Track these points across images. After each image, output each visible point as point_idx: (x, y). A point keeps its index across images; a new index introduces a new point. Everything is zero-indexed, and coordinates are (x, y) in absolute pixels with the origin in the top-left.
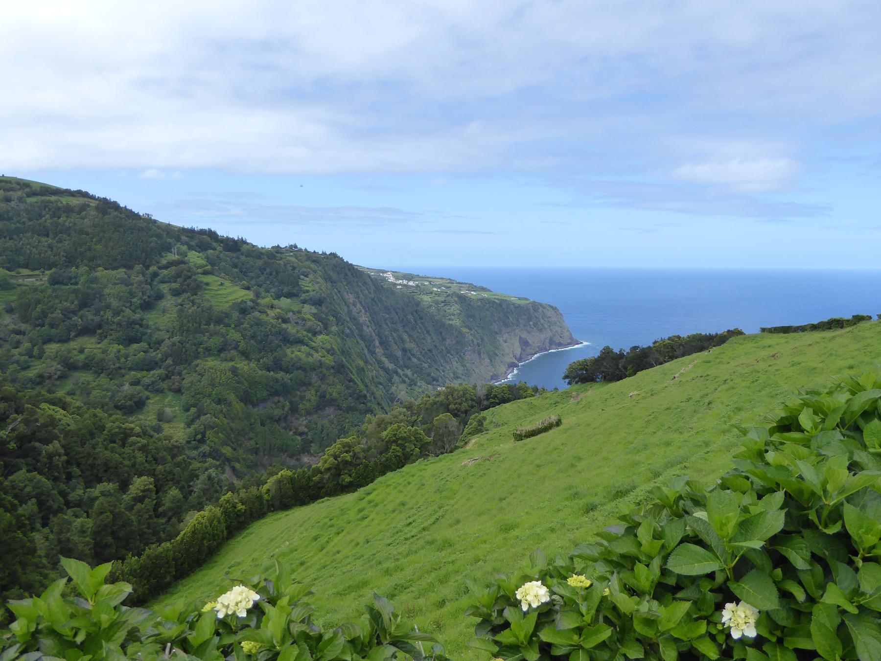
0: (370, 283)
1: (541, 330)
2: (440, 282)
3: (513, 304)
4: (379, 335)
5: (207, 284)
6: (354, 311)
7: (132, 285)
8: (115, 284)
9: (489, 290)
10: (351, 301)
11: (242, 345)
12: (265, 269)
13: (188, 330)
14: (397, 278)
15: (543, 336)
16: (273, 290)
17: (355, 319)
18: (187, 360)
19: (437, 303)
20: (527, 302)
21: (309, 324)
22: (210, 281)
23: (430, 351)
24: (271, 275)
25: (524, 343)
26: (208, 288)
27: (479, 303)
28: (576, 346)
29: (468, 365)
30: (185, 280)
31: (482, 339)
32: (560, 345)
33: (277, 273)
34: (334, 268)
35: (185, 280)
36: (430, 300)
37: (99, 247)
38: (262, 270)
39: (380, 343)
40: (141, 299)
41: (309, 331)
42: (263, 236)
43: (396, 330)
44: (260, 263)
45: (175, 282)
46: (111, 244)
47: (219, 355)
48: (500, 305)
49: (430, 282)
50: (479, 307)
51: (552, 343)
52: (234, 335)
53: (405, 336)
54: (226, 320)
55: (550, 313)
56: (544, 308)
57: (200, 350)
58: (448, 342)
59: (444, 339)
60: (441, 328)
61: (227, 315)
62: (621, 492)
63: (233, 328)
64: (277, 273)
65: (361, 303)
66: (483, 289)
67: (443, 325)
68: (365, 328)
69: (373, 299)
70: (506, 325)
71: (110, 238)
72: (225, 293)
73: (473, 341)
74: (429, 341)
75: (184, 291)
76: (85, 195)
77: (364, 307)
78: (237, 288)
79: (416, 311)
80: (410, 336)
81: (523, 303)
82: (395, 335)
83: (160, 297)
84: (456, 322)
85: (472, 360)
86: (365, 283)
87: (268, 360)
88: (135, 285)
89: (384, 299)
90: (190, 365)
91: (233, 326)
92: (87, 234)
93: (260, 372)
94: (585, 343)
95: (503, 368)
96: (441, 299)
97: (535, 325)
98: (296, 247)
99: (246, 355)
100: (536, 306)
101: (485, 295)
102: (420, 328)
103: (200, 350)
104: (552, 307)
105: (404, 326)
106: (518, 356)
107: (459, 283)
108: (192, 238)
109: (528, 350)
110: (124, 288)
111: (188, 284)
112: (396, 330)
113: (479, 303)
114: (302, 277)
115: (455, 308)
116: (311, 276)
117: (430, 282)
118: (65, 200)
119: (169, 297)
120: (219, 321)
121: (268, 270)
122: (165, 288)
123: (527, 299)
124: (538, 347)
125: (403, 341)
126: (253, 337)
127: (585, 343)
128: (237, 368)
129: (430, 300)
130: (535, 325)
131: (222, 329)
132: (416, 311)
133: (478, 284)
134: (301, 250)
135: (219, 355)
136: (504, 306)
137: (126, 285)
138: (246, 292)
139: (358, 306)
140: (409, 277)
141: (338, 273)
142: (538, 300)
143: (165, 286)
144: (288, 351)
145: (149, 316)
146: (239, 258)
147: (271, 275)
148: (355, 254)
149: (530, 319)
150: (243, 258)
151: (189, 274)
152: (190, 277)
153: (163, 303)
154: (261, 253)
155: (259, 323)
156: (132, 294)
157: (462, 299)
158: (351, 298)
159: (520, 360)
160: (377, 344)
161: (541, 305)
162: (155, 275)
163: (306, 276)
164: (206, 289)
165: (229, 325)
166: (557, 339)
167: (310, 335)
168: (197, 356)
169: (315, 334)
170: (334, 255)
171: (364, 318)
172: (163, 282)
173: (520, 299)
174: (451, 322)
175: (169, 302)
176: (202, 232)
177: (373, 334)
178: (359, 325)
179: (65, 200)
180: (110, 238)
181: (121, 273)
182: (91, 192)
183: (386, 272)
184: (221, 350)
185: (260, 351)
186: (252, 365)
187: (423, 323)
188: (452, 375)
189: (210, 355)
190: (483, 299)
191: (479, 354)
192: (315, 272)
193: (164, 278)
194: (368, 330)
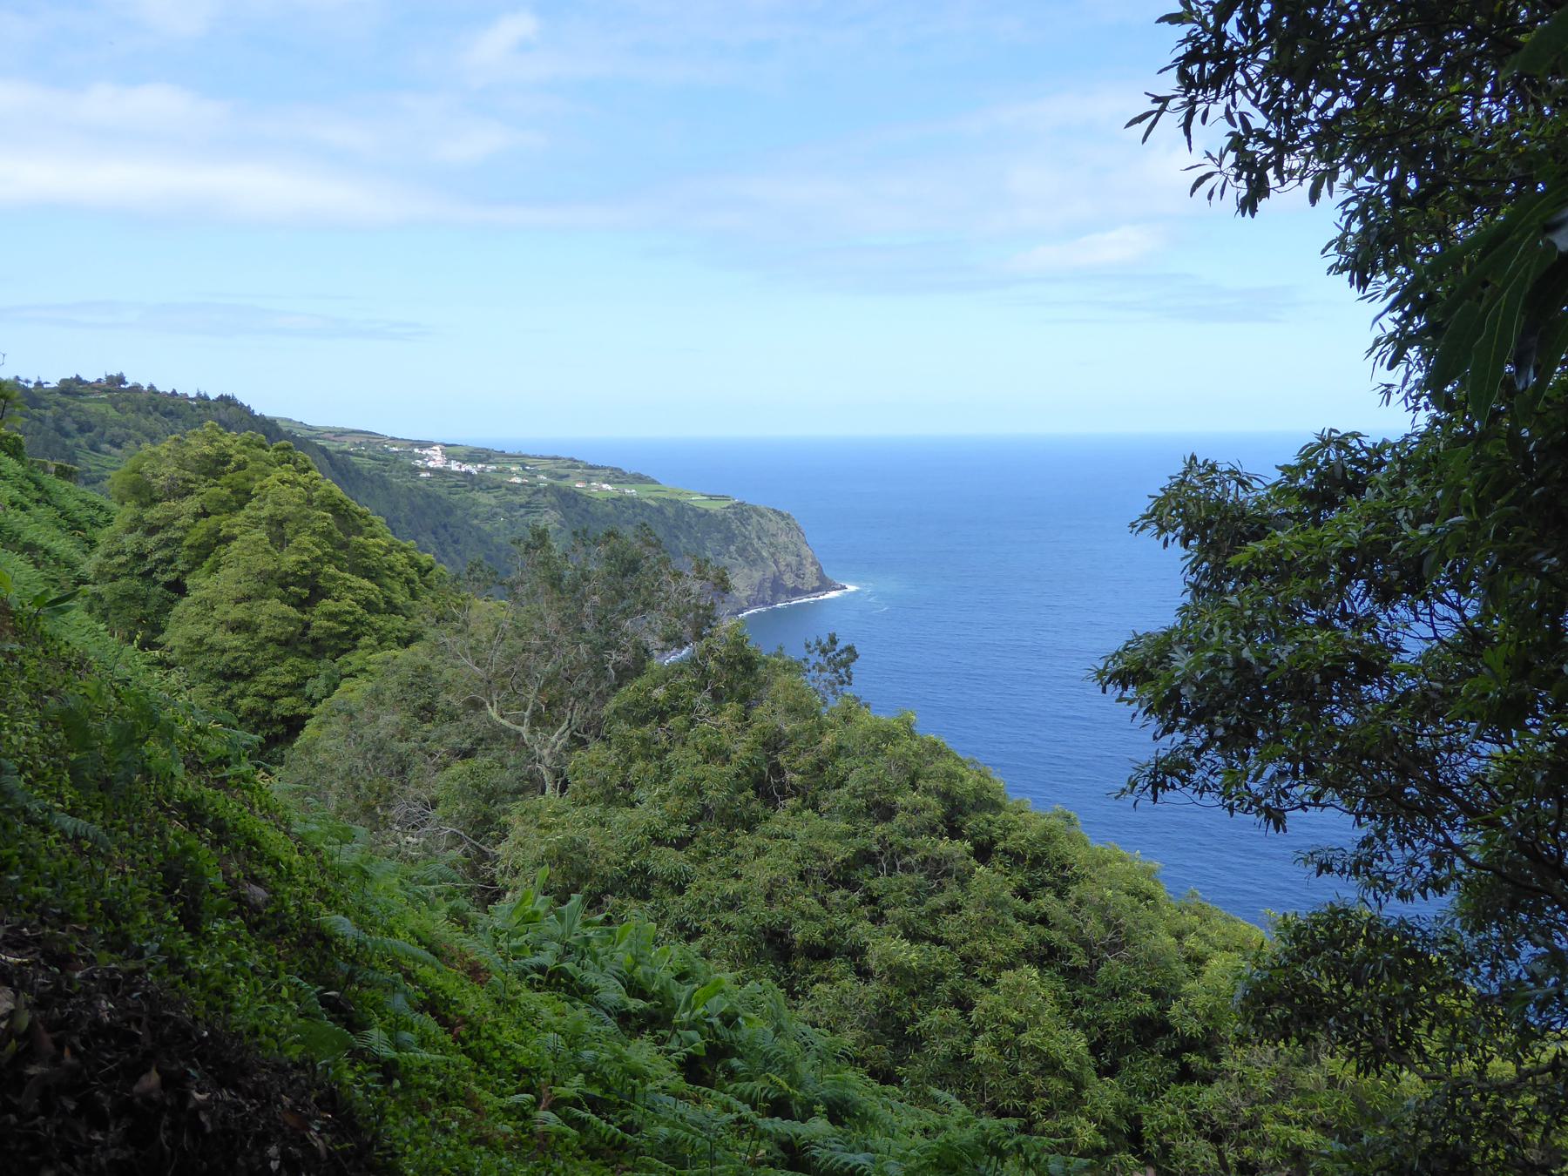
1: (752, 564)
2: (550, 465)
3: (693, 509)
9: (654, 482)
15: (757, 575)
19: (510, 508)
20: (726, 504)
27: (610, 508)
28: (832, 594)
32: (796, 592)
36: (494, 502)
48: (660, 510)
50: (608, 515)
51: (777, 588)
62: (569, 990)
66: (639, 479)
79: (445, 526)
81: (715, 507)
94: (851, 588)
96: (518, 499)
98: (121, 379)
100: (743, 512)
104: (779, 513)
107: (592, 468)
113: (610, 508)
123: (725, 498)
124: (747, 599)
127: (851, 588)
129: (494, 502)
130: (742, 552)
132: (445, 526)
133: (629, 468)
136: (670, 512)
140: (475, 455)
142: (750, 500)
148: (268, 398)
157: (568, 500)
160: (1262, 546)
161: (755, 510)
166: (789, 581)
170: (227, 401)
173: (711, 498)
187: (458, 552)
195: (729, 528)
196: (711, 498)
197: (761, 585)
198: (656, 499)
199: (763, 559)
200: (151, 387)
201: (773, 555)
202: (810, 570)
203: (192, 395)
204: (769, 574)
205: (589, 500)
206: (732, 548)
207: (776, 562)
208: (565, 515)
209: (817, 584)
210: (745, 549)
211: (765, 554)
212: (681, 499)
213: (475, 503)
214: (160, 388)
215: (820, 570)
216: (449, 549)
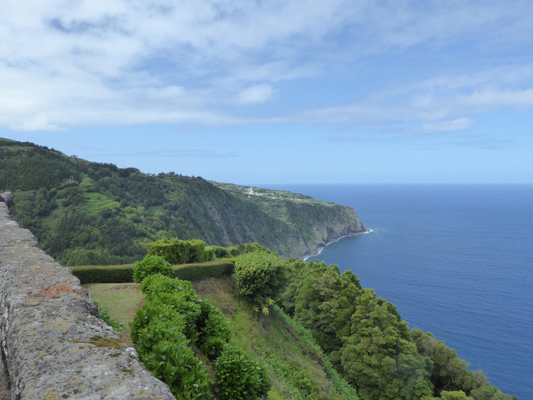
0: (224, 195)
1: (342, 223)
2: (282, 193)
3: (324, 207)
4: (227, 228)
5: (89, 198)
6: (210, 212)
7: (35, 200)
8: (25, 200)
9: (312, 198)
10: (209, 206)
11: (100, 238)
12: (142, 188)
13: (65, 229)
14: (255, 191)
15: (343, 227)
16: (146, 201)
17: (210, 218)
18: (60, 249)
19: (273, 206)
20: (333, 205)
21: (155, 223)
22: (91, 196)
23: (263, 237)
24: (146, 191)
25: (330, 231)
26: (88, 201)
27: (300, 206)
29: (289, 245)
30: (72, 196)
31: (301, 229)
32: (355, 232)
33: (150, 190)
34: (200, 187)
35: (72, 196)
36: (268, 205)
37: (21, 176)
38: (140, 188)
39: (228, 233)
40: (39, 209)
41: (154, 227)
42: (150, 167)
43: (240, 224)
44: (140, 184)
45: (66, 198)
46: (29, 174)
47: (84, 245)
48: (315, 207)
49: (275, 193)
52: (96, 231)
53: (246, 228)
54: (93, 222)
55: (348, 212)
56: (344, 209)
57: (71, 242)
58: (277, 231)
59: (274, 229)
60: (272, 223)
61: (94, 219)
63: (97, 227)
64: (150, 190)
65: (215, 207)
66: (308, 197)
67: (274, 221)
68: (217, 223)
69: (225, 205)
70: (319, 220)
71: (29, 171)
72: (101, 203)
73: (293, 230)
74: (263, 231)
75: (71, 203)
76: (32, 145)
77: (217, 210)
78: (111, 200)
80: (249, 227)
81: (331, 206)
82: (238, 227)
83: (55, 207)
84: (284, 219)
85: (292, 242)
86: (220, 195)
87: (117, 248)
88: (37, 200)
89: (233, 204)
90: (62, 252)
91: (96, 225)
92: (16, 168)
93: (110, 256)
95: (314, 247)
97: (338, 219)
99: (103, 245)
100: (339, 208)
101: (306, 201)
102: (258, 223)
103: (71, 242)
105: (246, 222)
106: (326, 239)
108: (96, 170)
109: (333, 235)
110: (29, 202)
111: (76, 198)
112: (240, 224)
113: (300, 206)
114: (170, 192)
115: (284, 210)
116: (176, 191)
117: (275, 193)
118: (11, 149)
119: (61, 207)
120: (87, 223)
121: (144, 188)
122: (59, 202)
125: (245, 231)
126: (109, 233)
127: (371, 231)
128: (93, 254)
129: (268, 205)
130: (338, 219)
131: (89, 228)
134: (177, 175)
135: (84, 245)
136: (317, 207)
137: (31, 200)
138: (117, 203)
139: (214, 209)
140: (261, 191)
141: (201, 189)
143: (60, 200)
144: (135, 242)
145: (45, 220)
146: (126, 181)
147: (146, 191)
149: (335, 215)
150: (129, 181)
151: (75, 192)
152: (75, 194)
153: (55, 212)
154: (143, 178)
155: (116, 223)
156: (33, 206)
157: (289, 204)
158: (209, 205)
159: (327, 241)
160: (225, 233)
161: (342, 207)
162: (55, 193)
163: (173, 192)
164: (86, 202)
165: (94, 225)
166: (353, 228)
167: (153, 230)
168: (68, 246)
169: (158, 229)
170: (199, 178)
171: (217, 217)
172: (59, 198)
173: (329, 203)
174: (280, 219)
175: (60, 212)
176: (106, 165)
177: (223, 227)
178: (213, 222)
179: (11, 149)
180: (29, 171)
181: (31, 193)
182: (36, 143)
183: (249, 187)
184: (86, 242)
185: (113, 242)
186: (106, 251)
187: (258, 219)
188: (277, 252)
189: (78, 245)
190: (303, 204)
191: (298, 238)
192: (181, 189)
193: (59, 195)
194: (219, 225)
195: (334, 212)
196: (329, 203)
197: (344, 229)
198: (314, 204)
199: (345, 222)
200: (181, 175)
201: (348, 220)
202: (359, 225)
203: (191, 177)
204: (347, 226)
205: (295, 204)
206: (336, 218)
207: (349, 223)
208: (288, 208)
209: (361, 229)
210: (339, 219)
211: (345, 220)
212: (321, 203)
213: (263, 205)
214: (183, 175)
215: (362, 225)
216: (257, 219)
